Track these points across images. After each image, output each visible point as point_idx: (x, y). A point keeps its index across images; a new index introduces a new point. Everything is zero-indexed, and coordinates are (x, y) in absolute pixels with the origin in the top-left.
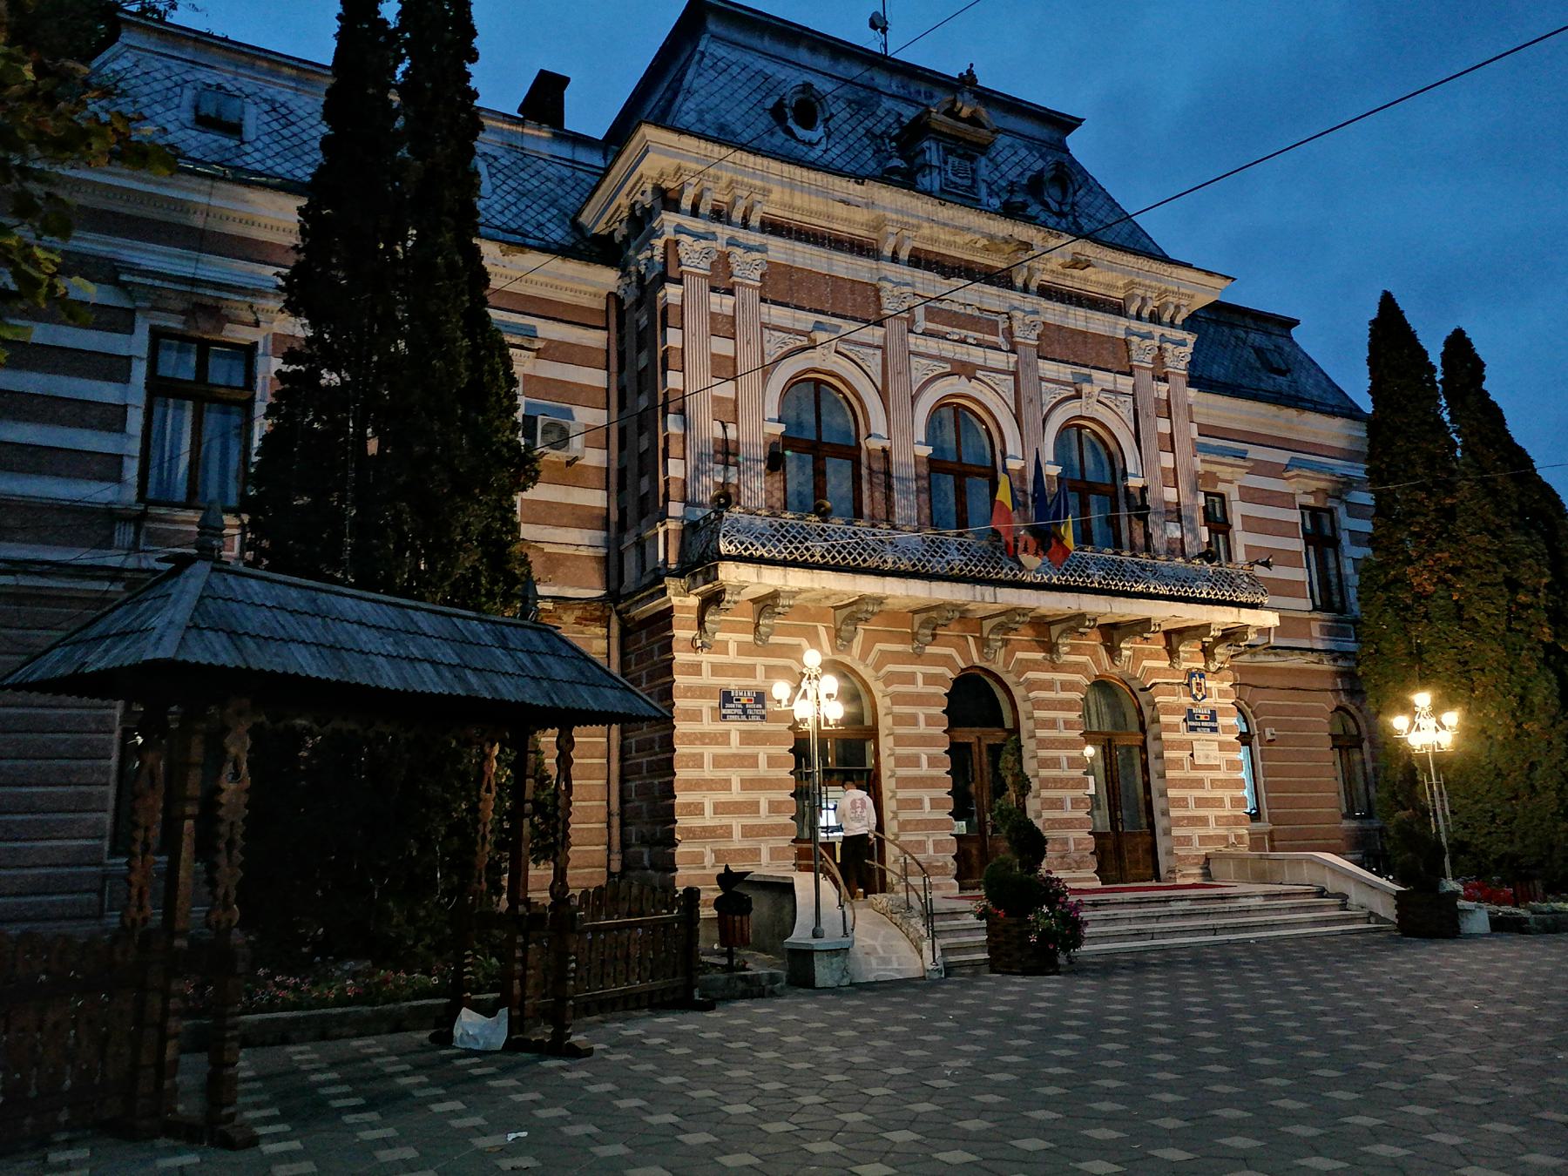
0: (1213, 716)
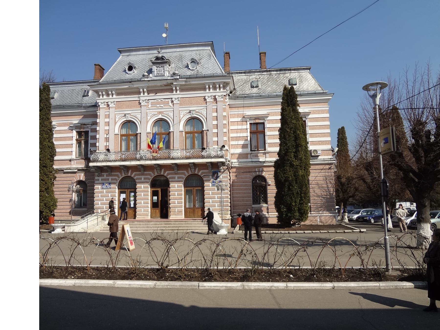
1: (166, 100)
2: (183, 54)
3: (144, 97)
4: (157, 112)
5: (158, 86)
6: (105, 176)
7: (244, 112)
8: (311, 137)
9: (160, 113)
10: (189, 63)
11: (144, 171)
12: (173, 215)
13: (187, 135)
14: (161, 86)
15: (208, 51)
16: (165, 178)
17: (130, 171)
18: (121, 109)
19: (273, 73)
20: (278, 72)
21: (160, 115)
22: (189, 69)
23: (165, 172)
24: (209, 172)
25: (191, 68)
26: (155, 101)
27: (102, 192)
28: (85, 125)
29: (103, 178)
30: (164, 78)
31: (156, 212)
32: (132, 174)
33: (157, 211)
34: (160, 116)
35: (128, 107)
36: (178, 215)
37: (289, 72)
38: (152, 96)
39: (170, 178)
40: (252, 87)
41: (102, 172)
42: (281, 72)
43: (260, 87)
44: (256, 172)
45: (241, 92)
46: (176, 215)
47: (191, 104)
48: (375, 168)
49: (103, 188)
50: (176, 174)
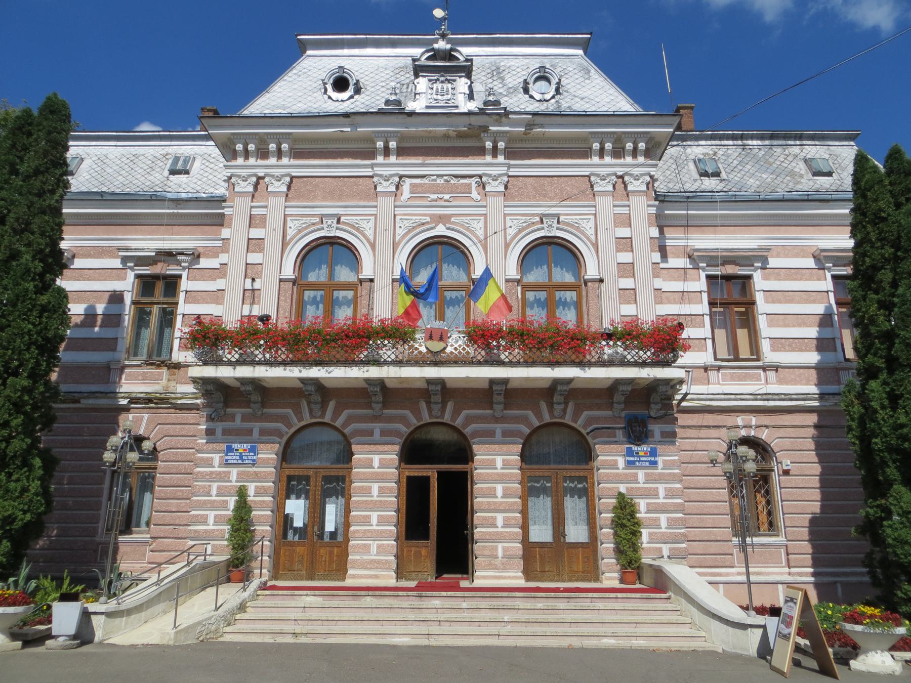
2: (504, 63)
3: (387, 167)
4: (431, 216)
5: (435, 138)
6: (238, 418)
7: (691, 243)
8: (774, 349)
9: (441, 219)
11: (385, 405)
12: (484, 569)
13: (530, 295)
14: (446, 136)
15: (577, 60)
17: (332, 405)
18: (308, 199)
19: (750, 142)
20: (767, 142)
22: (531, 97)
23: (456, 413)
26: (425, 181)
27: (225, 477)
29: (228, 425)
31: (418, 555)
33: (424, 552)
34: (441, 230)
35: (331, 195)
36: (504, 569)
37: (798, 143)
38: (413, 165)
39: (476, 434)
40: (704, 174)
41: (226, 404)
42: (775, 142)
43: (724, 175)
44: (738, 427)
45: (670, 185)
46: (496, 568)
47: (545, 196)
49: (227, 464)
50: (497, 420)
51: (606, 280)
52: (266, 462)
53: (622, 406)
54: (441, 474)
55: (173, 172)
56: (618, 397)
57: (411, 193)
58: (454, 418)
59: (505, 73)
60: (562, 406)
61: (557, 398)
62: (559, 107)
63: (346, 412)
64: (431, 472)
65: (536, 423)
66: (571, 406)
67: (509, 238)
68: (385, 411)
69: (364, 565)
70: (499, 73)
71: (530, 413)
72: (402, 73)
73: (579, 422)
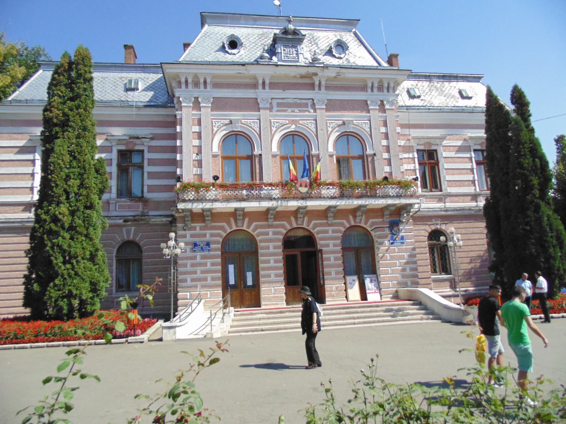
0: (208, 244)
1: (304, 101)
6: (198, 228)
10: (332, 47)
16: (306, 234)
17: (246, 220)
21: (294, 126)
24: (383, 222)
25: (337, 55)
28: (138, 138)
29: (193, 232)
30: (298, 64)
32: (249, 227)
34: (293, 128)
39: (318, 233)
48: (69, 328)
50: (329, 225)
51: (377, 154)
52: (216, 250)
53: (273, 220)
54: (302, 253)
55: (127, 90)
56: (387, 213)
57: (278, 107)
58: (308, 225)
59: (317, 40)
60: (360, 217)
61: (300, 215)
62: (349, 62)
63: (254, 224)
64: (297, 252)
65: (289, 228)
66: (306, 219)
67: (329, 132)
68: (274, 223)
69: (269, 299)
70: (314, 40)
71: (344, 221)
72: (263, 38)
73: (310, 227)
